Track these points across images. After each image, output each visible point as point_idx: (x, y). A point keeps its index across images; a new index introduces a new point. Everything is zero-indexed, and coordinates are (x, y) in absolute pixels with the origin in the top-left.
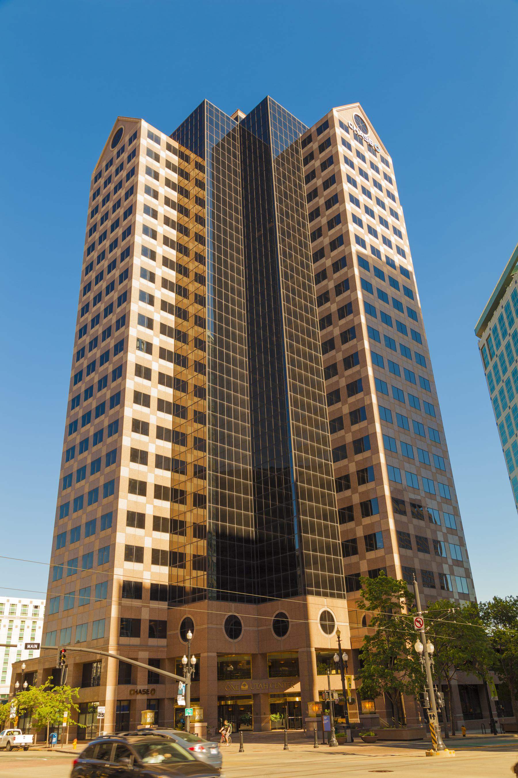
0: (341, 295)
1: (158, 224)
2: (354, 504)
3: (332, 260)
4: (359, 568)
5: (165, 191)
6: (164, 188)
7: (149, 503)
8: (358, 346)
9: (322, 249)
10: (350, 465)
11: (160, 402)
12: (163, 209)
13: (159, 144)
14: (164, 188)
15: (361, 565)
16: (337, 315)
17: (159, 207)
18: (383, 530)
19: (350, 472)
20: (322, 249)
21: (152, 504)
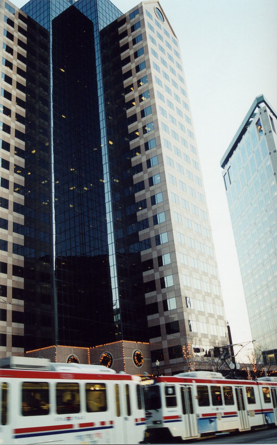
0: (134, 32)
1: (8, 278)
2: (153, 258)
3: (137, 78)
4: (157, 299)
5: (18, 35)
6: (17, 33)
7: (9, 279)
8: (140, 18)
9: (126, 31)
10: (155, 274)
11: (17, 131)
12: (14, 108)
13: (13, 40)
14: (17, 33)
15: (160, 320)
16: (133, 56)
17: (14, 46)
18: (158, 154)
19: (149, 217)
20: (126, 31)
21: (11, 279)
